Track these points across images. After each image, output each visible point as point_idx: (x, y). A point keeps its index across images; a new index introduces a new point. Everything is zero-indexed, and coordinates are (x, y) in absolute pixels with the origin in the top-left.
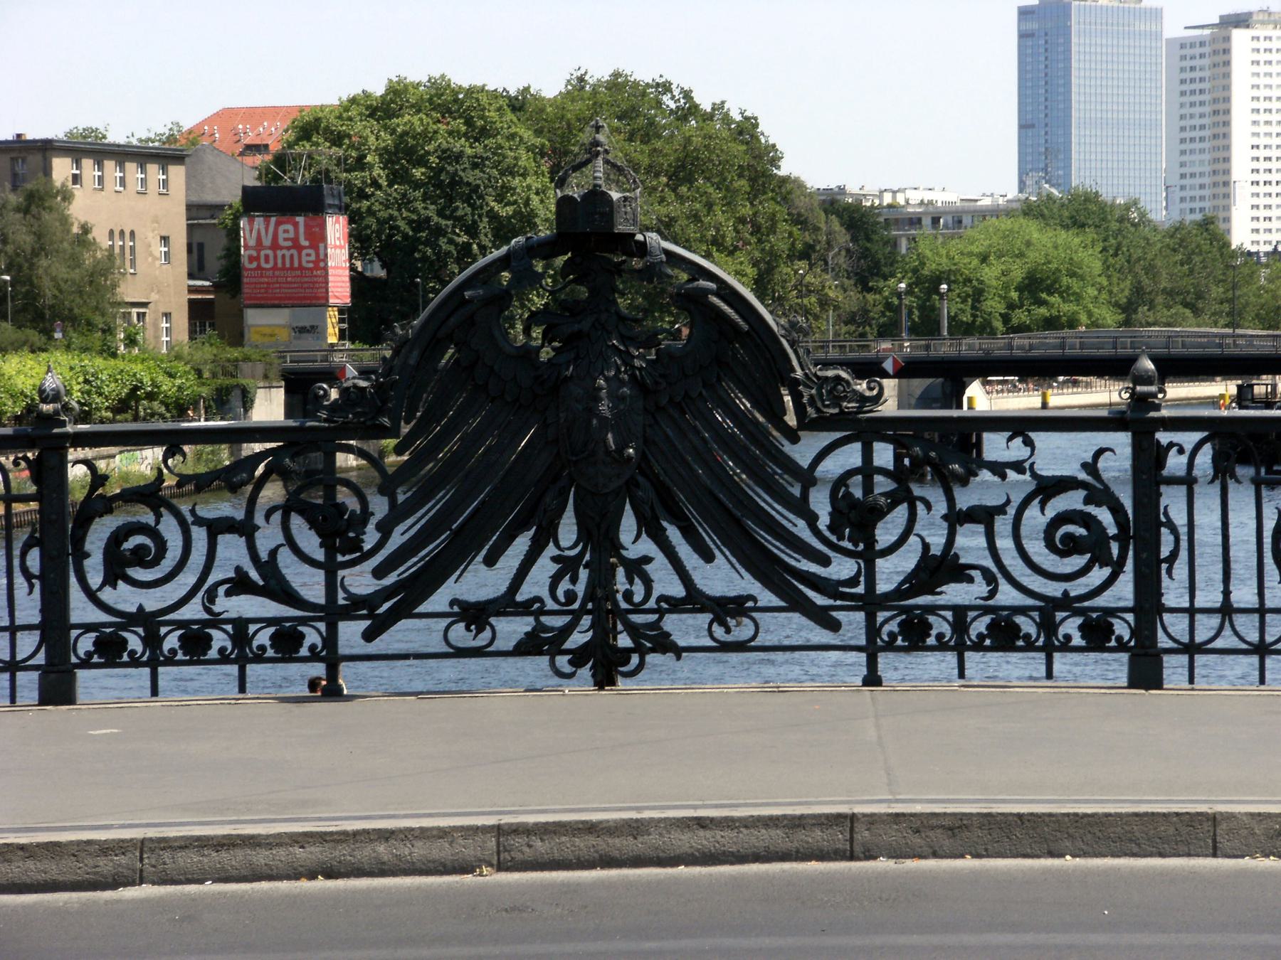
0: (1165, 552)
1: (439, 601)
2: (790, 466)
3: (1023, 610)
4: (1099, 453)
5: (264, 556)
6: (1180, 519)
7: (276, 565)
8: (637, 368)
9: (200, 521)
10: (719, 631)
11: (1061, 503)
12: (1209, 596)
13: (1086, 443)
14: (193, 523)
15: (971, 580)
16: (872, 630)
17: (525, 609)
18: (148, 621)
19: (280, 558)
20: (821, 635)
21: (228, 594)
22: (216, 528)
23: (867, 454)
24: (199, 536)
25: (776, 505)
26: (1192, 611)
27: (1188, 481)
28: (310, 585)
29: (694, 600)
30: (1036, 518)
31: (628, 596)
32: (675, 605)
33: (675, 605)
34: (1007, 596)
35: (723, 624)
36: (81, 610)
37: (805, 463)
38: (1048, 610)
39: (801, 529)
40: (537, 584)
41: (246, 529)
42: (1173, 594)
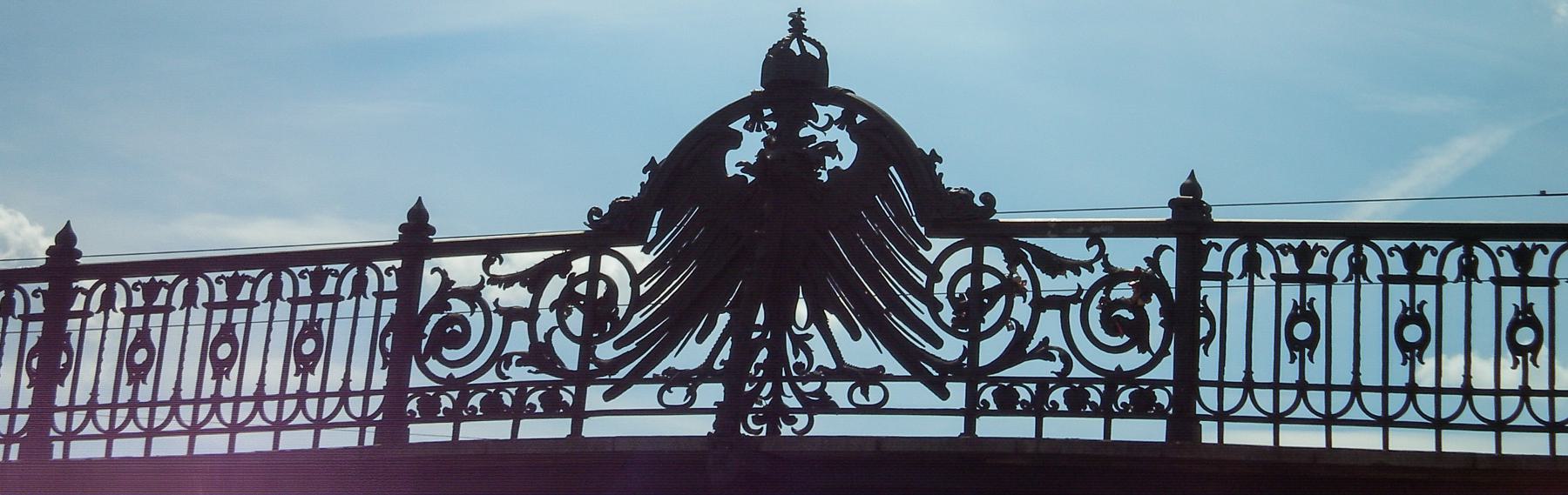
0: (1203, 333)
2: (921, 263)
6: (1214, 306)
9: (499, 310)
12: (1235, 372)
13: (1148, 245)
14: (495, 312)
15: (1053, 358)
16: (972, 396)
18: (464, 387)
19: (97, 308)
21: (519, 364)
22: (511, 315)
23: (978, 256)
24: (498, 321)
25: (910, 297)
26: (1221, 385)
27: (1224, 277)
28: (568, 352)
29: (843, 372)
32: (826, 375)
33: (826, 375)
34: (1078, 371)
36: (417, 379)
38: (1114, 379)
39: (925, 316)
42: (1207, 367)
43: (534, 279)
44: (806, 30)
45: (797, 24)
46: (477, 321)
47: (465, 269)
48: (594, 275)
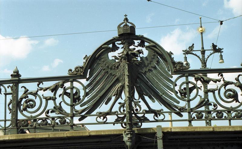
1: (94, 113)
3: (224, 111)
4: (239, 76)
5: (164, 114)
7: (214, 45)
8: (85, 91)
10: (156, 118)
11: (229, 87)
16: (190, 116)
17: (114, 113)
20: (178, 118)
22: (47, 99)
23: (187, 79)
24: (44, 101)
28: (67, 109)
29: (151, 111)
30: (223, 90)
31: (137, 110)
32: (147, 112)
35: (157, 116)
37: (174, 81)
39: (174, 95)
40: (116, 108)
41: (54, 99)
43: (54, 89)
44: (128, 20)
45: (126, 19)
46: (38, 101)
47: (32, 87)
48: (72, 88)
